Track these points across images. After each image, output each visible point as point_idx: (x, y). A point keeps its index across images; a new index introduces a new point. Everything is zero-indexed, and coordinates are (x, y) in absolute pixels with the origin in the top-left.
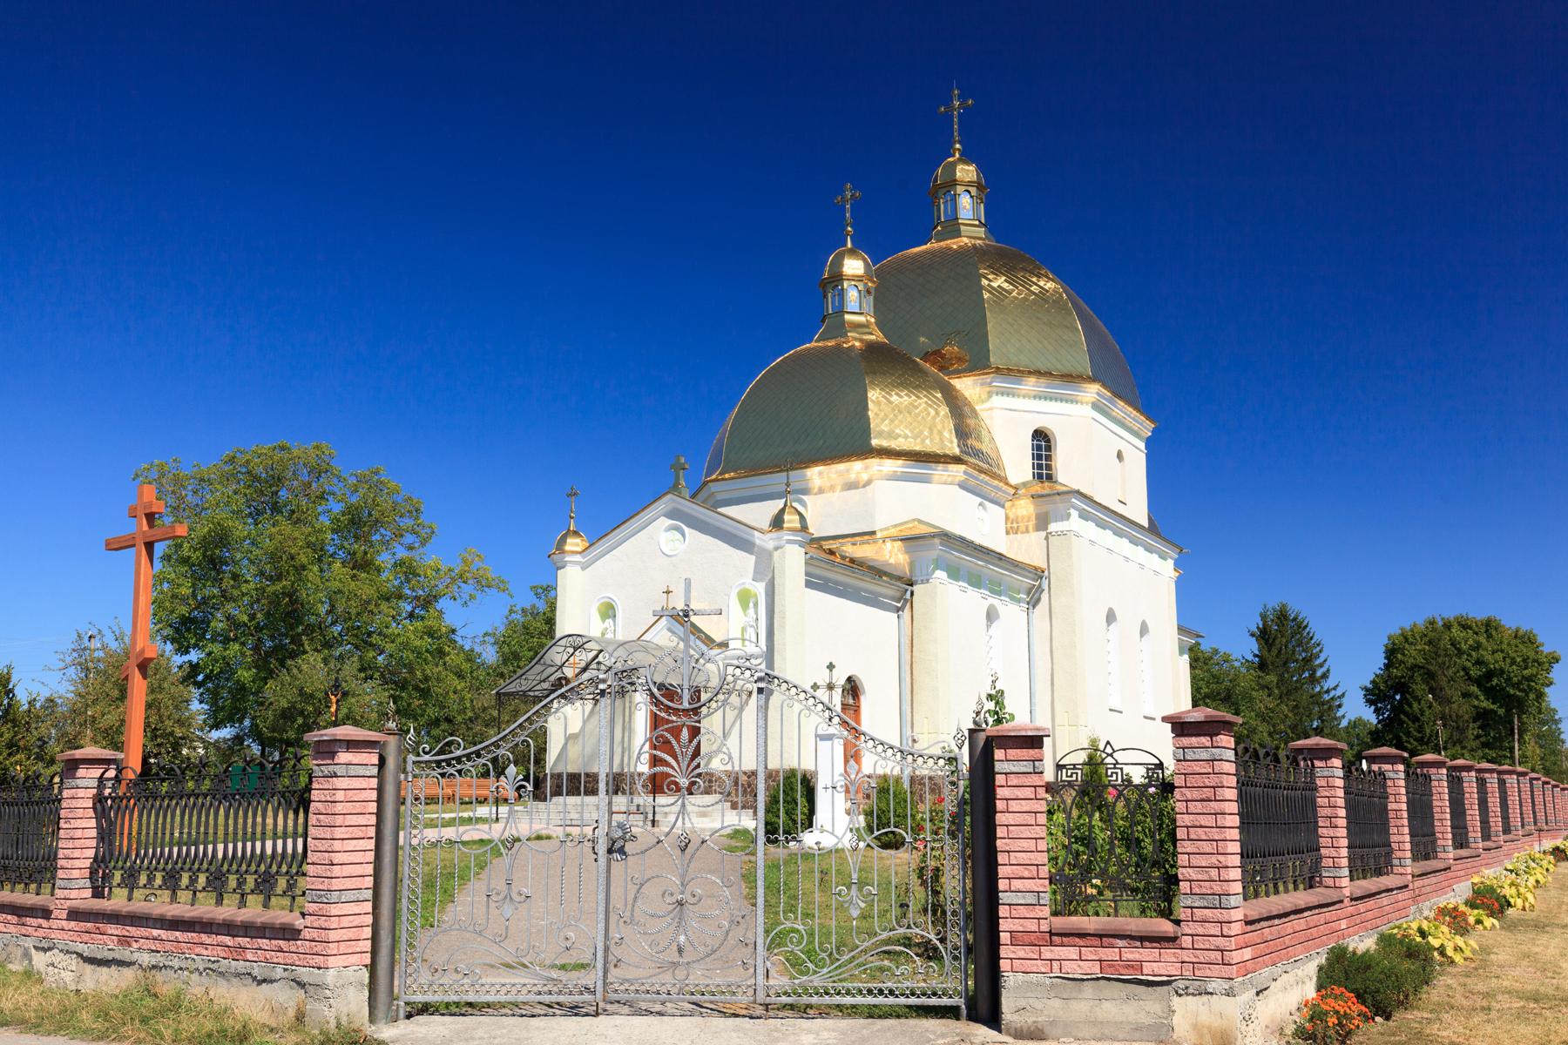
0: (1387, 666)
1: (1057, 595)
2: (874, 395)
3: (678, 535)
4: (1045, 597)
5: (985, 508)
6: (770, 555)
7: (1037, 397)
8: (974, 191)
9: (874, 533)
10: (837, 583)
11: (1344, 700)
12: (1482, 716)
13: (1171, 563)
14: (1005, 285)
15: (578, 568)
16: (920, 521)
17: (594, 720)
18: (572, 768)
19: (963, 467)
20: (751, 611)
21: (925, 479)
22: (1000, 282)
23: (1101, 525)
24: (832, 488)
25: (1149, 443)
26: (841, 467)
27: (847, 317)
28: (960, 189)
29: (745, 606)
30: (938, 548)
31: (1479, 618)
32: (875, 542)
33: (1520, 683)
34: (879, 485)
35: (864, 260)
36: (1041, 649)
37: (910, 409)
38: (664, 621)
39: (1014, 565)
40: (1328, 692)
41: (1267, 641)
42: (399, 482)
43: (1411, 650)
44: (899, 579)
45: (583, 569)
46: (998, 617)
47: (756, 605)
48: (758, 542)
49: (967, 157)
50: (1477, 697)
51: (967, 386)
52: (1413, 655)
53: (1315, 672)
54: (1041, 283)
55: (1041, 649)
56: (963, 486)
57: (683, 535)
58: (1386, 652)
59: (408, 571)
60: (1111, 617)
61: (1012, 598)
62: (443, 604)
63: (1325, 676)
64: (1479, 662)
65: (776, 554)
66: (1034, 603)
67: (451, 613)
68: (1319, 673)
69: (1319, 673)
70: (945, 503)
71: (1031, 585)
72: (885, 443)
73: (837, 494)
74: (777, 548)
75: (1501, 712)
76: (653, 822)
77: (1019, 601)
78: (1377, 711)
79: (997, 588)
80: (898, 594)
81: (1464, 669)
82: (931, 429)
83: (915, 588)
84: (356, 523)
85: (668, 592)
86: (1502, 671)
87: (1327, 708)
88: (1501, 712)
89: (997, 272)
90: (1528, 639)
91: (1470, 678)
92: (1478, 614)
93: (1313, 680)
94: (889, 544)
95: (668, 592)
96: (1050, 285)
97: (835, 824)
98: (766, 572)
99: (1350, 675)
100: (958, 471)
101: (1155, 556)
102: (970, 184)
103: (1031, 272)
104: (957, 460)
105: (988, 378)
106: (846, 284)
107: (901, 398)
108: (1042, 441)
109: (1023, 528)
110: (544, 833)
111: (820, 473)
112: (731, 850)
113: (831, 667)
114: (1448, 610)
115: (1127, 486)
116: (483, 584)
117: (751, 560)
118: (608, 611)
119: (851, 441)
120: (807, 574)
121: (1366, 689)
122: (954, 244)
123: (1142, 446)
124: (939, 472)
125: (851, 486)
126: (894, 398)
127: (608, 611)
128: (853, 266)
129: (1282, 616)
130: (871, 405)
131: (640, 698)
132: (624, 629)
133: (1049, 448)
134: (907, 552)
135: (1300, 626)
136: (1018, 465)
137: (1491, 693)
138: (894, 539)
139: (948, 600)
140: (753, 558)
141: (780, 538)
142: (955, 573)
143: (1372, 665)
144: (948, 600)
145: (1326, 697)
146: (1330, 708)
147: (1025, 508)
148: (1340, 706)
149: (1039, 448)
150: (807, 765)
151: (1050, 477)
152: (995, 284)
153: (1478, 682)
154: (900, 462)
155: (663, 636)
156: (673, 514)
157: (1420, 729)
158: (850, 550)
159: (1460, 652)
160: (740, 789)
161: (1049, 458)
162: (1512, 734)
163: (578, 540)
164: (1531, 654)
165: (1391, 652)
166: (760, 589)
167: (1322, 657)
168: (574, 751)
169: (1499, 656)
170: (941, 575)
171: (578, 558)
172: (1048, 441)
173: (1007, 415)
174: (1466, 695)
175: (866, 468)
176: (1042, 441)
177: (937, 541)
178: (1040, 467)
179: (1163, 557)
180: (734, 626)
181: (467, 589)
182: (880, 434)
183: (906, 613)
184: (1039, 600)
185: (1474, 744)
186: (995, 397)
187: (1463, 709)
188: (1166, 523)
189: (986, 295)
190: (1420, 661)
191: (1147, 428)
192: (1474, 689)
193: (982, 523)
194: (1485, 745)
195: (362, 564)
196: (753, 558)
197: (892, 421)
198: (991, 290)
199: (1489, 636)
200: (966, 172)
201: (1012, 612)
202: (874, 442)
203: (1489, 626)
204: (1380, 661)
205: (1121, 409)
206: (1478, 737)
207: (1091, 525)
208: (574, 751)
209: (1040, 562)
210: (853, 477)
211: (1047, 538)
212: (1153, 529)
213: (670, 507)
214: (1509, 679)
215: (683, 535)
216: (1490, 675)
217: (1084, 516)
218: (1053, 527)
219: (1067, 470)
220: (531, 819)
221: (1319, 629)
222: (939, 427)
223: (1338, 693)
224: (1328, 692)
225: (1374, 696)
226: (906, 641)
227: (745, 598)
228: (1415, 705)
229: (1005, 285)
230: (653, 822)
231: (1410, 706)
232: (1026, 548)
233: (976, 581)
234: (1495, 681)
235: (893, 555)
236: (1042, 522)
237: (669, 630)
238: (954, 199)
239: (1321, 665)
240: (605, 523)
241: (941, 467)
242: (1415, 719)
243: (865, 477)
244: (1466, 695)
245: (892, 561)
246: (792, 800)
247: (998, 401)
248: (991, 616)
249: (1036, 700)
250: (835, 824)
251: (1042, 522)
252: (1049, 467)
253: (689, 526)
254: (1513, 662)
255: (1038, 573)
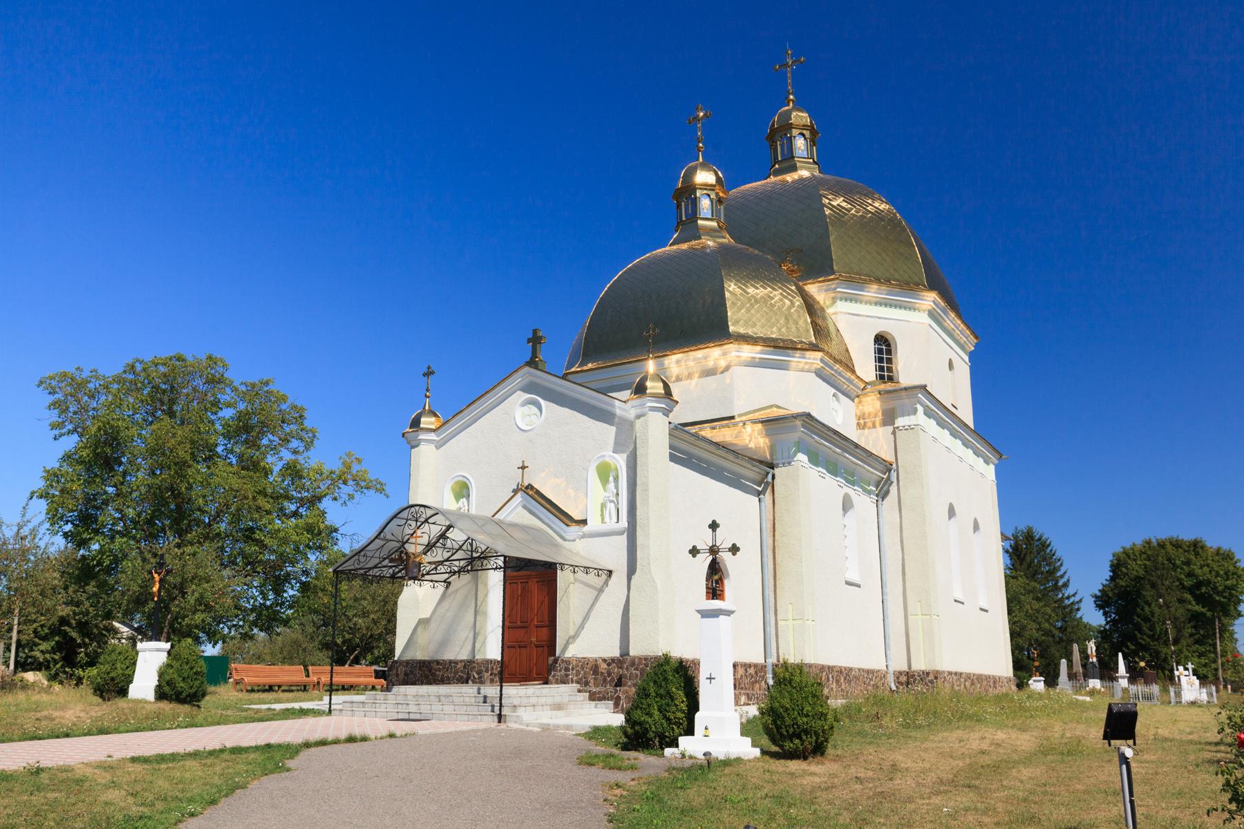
0: (1112, 579)
1: (906, 486)
2: (731, 288)
3: (534, 409)
4: (893, 489)
5: (838, 400)
6: (632, 424)
7: (879, 303)
8: (807, 133)
9: (733, 418)
10: (700, 459)
11: (1082, 605)
12: (1195, 618)
13: (992, 467)
14: (844, 204)
15: (432, 447)
16: (778, 407)
17: (446, 604)
18: (420, 655)
19: (819, 355)
20: (611, 485)
21: (783, 366)
22: (839, 201)
23: (941, 424)
24: (690, 376)
25: (972, 356)
26: (699, 354)
27: (700, 222)
28: (795, 132)
29: (604, 481)
30: (800, 431)
31: (1185, 539)
32: (735, 425)
33: (1223, 591)
34: (737, 371)
35: (716, 174)
36: (891, 539)
37: (766, 299)
38: (519, 494)
39: (868, 456)
40: (1068, 598)
41: (1019, 556)
42: (291, 388)
43: (1132, 564)
44: (761, 462)
45: (437, 448)
46: (852, 506)
47: (616, 479)
48: (618, 412)
49: (799, 106)
50: (1190, 603)
51: (812, 288)
52: (1136, 568)
53: (1057, 582)
54: (876, 204)
55: (891, 539)
56: (819, 374)
57: (540, 408)
58: (1111, 566)
59: (293, 472)
60: (952, 512)
61: (864, 490)
62: (326, 504)
63: (1066, 585)
64: (1190, 575)
65: (638, 423)
66: (883, 495)
67: (333, 512)
68: (1060, 583)
69: (1060, 583)
70: (799, 388)
71: (881, 478)
72: (742, 331)
73: (695, 380)
74: (638, 417)
75: (1209, 614)
76: (500, 718)
77: (869, 492)
78: (1105, 614)
79: (852, 478)
80: (758, 477)
81: (1179, 579)
82: (786, 318)
83: (777, 471)
84: (246, 429)
85: (523, 468)
86: (1208, 582)
87: (1068, 611)
88: (1209, 614)
89: (837, 194)
90: (1228, 556)
91: (1184, 587)
92: (1187, 536)
93: (1056, 588)
94: (749, 428)
95: (523, 468)
96: (883, 206)
97: (722, 729)
98: (628, 443)
99: (1085, 580)
100: (815, 358)
101: (981, 460)
102: (805, 127)
103: (866, 195)
104: (814, 348)
105: (833, 285)
106: (698, 193)
107: (757, 291)
108: (884, 345)
109: (870, 424)
110: (357, 732)
111: (678, 362)
112: (588, 761)
113: (714, 526)
114: (1161, 530)
115: (956, 390)
116: (363, 485)
117: (608, 432)
118: (462, 490)
119: (708, 326)
120: (671, 447)
121: (1096, 596)
122: (789, 178)
123: (966, 358)
124: (796, 359)
125: (709, 373)
126: (751, 290)
127: (462, 490)
128: (704, 177)
129: (1029, 536)
130: (727, 294)
131: (494, 580)
132: (477, 506)
133: (889, 352)
134: (768, 435)
135: (1044, 545)
136: (866, 368)
137: (1200, 599)
138: (754, 422)
139: (808, 484)
140: (613, 429)
141: (643, 405)
142: (815, 459)
143: (1103, 575)
144: (808, 484)
145: (1067, 602)
146: (1071, 611)
147: (872, 404)
148: (1078, 609)
149: (880, 351)
150: (680, 650)
151: (891, 379)
152: (834, 203)
153: (1191, 590)
154: (759, 348)
155: (517, 513)
156: (527, 389)
157: (1152, 628)
158: (707, 432)
159: (1175, 567)
160: (602, 679)
161: (889, 361)
162: (1215, 634)
163: (433, 419)
164: (1231, 568)
165: (1117, 567)
166: (620, 461)
167: (1063, 570)
168: (423, 638)
169: (1206, 569)
170: (802, 458)
171: (432, 436)
172: (889, 345)
173: (856, 316)
174: (1181, 601)
175: (724, 354)
176: (884, 345)
177: (798, 423)
178: (881, 369)
179: (987, 462)
180: (592, 500)
181: (346, 490)
182: (736, 322)
183: (767, 497)
184: (888, 492)
185: (1190, 641)
186: (839, 303)
187: (1180, 612)
188: (990, 430)
189: (827, 212)
190: (1142, 573)
191: (971, 342)
192: (1188, 596)
193: (839, 414)
194: (1197, 642)
195: (252, 466)
196: (613, 429)
197: (748, 311)
198: (832, 208)
199: (1197, 554)
200: (800, 117)
201: (864, 502)
202: (732, 329)
203: (1196, 546)
204: (1107, 574)
205: (952, 320)
206: (1191, 635)
207: (933, 422)
208: (423, 638)
209: (888, 456)
210: (711, 364)
211: (894, 433)
212: (975, 432)
213: (526, 381)
214: (1215, 588)
215: (540, 408)
216: (1199, 584)
217: (929, 413)
218: (900, 422)
219: (907, 371)
220: (362, 712)
221: (1061, 547)
222: (795, 316)
223: (1077, 598)
224: (1068, 598)
225: (1103, 601)
226: (767, 526)
227: (605, 473)
228: (1147, 608)
229: (844, 204)
230: (500, 718)
231: (1143, 609)
232: (877, 441)
233: (834, 469)
234: (1204, 590)
235: (753, 438)
236: (889, 418)
237: (525, 507)
238: (790, 140)
239: (1062, 576)
240: (462, 401)
241: (798, 354)
242: (1146, 620)
243: (723, 364)
244: (1181, 601)
245: (752, 445)
246: (659, 698)
247: (842, 306)
248: (847, 505)
249: (888, 590)
250: (722, 729)
251: (889, 418)
252: (890, 370)
253: (545, 399)
254: (1218, 575)
255: (887, 467)
